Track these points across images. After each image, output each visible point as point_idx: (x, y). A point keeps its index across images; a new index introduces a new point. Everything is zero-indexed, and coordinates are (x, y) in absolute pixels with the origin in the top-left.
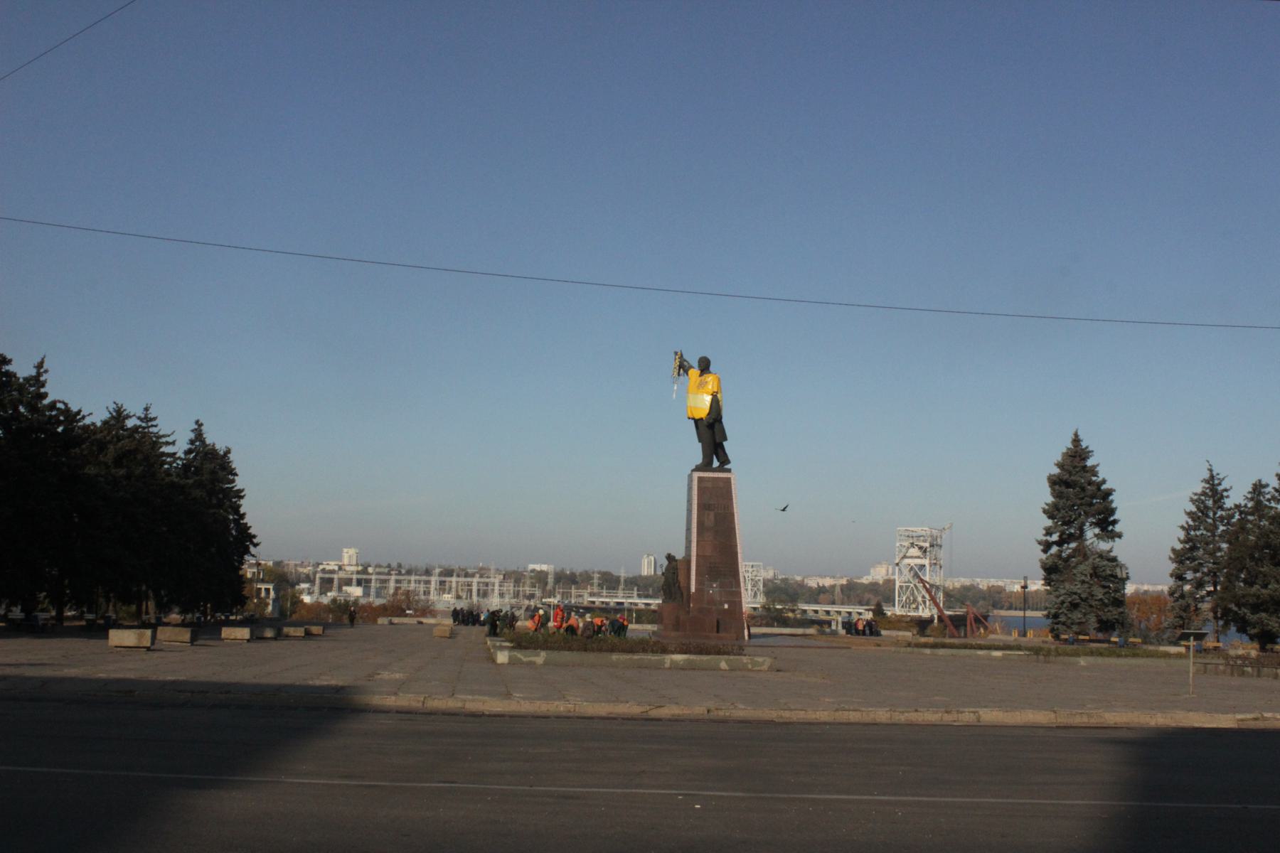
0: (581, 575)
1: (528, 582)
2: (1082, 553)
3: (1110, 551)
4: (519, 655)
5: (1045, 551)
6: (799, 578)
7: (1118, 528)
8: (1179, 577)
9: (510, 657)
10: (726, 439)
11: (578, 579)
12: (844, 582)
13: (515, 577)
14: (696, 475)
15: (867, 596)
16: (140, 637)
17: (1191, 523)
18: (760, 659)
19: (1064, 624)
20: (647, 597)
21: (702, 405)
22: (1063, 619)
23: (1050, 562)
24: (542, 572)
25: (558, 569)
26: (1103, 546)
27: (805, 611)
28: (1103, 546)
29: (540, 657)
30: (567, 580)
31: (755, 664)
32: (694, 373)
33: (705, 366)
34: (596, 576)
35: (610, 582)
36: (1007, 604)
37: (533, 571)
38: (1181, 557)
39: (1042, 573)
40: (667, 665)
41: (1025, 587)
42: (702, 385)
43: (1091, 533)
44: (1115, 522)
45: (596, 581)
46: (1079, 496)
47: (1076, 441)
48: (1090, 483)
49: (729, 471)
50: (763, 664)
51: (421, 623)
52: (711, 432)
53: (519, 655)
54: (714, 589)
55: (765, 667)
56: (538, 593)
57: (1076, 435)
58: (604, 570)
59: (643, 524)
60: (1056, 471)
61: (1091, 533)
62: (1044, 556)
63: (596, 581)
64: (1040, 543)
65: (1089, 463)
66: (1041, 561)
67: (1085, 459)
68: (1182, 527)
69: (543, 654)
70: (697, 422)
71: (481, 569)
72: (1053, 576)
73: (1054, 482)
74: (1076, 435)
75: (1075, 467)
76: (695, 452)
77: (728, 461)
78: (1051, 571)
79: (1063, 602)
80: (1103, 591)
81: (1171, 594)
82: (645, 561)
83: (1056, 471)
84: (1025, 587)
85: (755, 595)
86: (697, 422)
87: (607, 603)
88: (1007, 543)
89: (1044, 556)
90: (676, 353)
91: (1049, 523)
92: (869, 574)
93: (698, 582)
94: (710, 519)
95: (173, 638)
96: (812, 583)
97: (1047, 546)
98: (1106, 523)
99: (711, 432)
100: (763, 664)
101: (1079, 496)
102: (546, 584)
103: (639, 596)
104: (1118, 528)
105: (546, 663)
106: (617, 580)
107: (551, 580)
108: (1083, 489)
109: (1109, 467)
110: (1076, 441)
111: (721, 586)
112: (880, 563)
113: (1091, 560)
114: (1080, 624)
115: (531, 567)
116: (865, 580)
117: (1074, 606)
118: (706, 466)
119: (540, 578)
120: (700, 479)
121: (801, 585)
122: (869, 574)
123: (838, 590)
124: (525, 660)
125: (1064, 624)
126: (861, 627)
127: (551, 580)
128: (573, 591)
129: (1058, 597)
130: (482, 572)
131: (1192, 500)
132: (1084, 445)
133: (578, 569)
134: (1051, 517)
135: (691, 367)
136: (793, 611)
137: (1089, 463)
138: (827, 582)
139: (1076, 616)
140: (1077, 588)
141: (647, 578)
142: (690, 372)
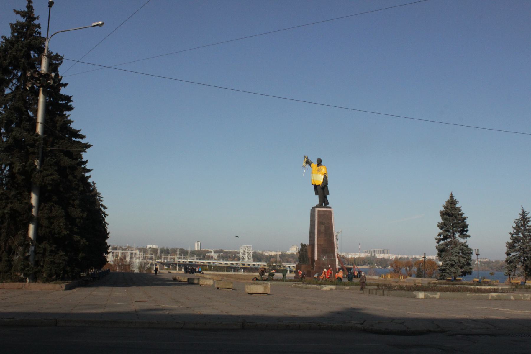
0: (171, 250)
1: (149, 252)
2: (455, 243)
3: (465, 243)
4: (429, 294)
5: (438, 243)
6: (260, 252)
7: (468, 233)
8: (508, 254)
9: (425, 295)
10: (328, 194)
11: (170, 251)
12: (280, 253)
13: (144, 250)
14: (317, 209)
15: (290, 259)
16: (266, 288)
17: (515, 231)
18: (526, 295)
19: (447, 273)
20: (200, 259)
21: (319, 179)
22: (447, 271)
23: (442, 247)
24: (154, 248)
25: (161, 247)
26: (462, 240)
27: (284, 266)
28: (462, 240)
29: (437, 295)
30: (166, 252)
31: (525, 297)
32: (314, 165)
33: (319, 163)
34: (178, 250)
35: (184, 253)
36: (347, 263)
37: (150, 248)
38: (511, 246)
39: (437, 252)
40: (490, 298)
41: (424, 258)
42: (319, 171)
43: (457, 235)
44: (467, 231)
45: (178, 252)
46: (453, 219)
47: (452, 197)
48: (459, 215)
49: (330, 207)
50: (527, 297)
51: (170, 272)
52: (322, 191)
53: (429, 294)
54: (324, 259)
55: (529, 298)
56: (154, 257)
57: (451, 194)
58: (181, 248)
59: (288, 231)
60: (443, 209)
61: (457, 235)
62: (437, 245)
63: (178, 252)
64: (436, 239)
65: (457, 206)
66: (437, 247)
67: (455, 205)
68: (510, 233)
69: (439, 293)
70: (316, 187)
71: (128, 247)
72: (443, 253)
73: (443, 214)
74: (451, 194)
75: (452, 208)
76: (315, 200)
77: (328, 204)
78: (441, 252)
79: (447, 264)
80: (463, 259)
81: (506, 261)
82: (196, 244)
83: (443, 209)
84: (424, 258)
85: (249, 258)
86: (316, 187)
87: (186, 262)
88: (422, 240)
89: (437, 245)
90: (305, 157)
91: (441, 231)
92: (289, 250)
93: (318, 256)
94: (323, 229)
95: (224, 287)
96: (267, 254)
97: (439, 240)
98: (463, 230)
99: (322, 191)
100: (527, 297)
101: (453, 219)
102: (157, 253)
103: (197, 259)
104: (468, 233)
105: (440, 298)
106: (187, 252)
107: (159, 252)
108: (456, 217)
109: (466, 208)
110: (452, 197)
111: (327, 257)
112: (293, 246)
113: (459, 246)
114: (454, 273)
115: (149, 246)
116: (288, 252)
117: (452, 265)
118: (320, 206)
119: (154, 251)
120: (319, 211)
121: (262, 255)
122: (289, 250)
123: (278, 257)
124: (431, 296)
125: (447, 273)
126: (356, 274)
127: (159, 252)
128: (169, 257)
129: (445, 262)
130: (129, 248)
131: (515, 222)
132: (455, 198)
133: (170, 247)
134: (441, 229)
135: (312, 163)
136: (280, 266)
137: (457, 206)
138: (273, 253)
139: (453, 269)
140: (454, 258)
141: (198, 251)
142: (312, 165)
